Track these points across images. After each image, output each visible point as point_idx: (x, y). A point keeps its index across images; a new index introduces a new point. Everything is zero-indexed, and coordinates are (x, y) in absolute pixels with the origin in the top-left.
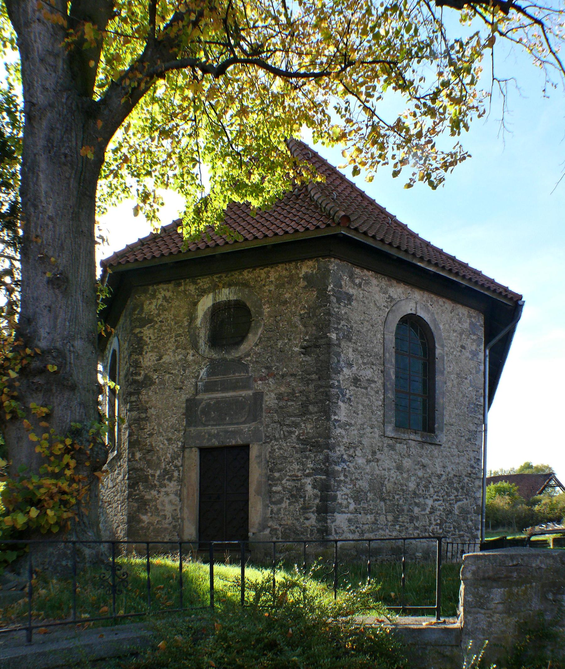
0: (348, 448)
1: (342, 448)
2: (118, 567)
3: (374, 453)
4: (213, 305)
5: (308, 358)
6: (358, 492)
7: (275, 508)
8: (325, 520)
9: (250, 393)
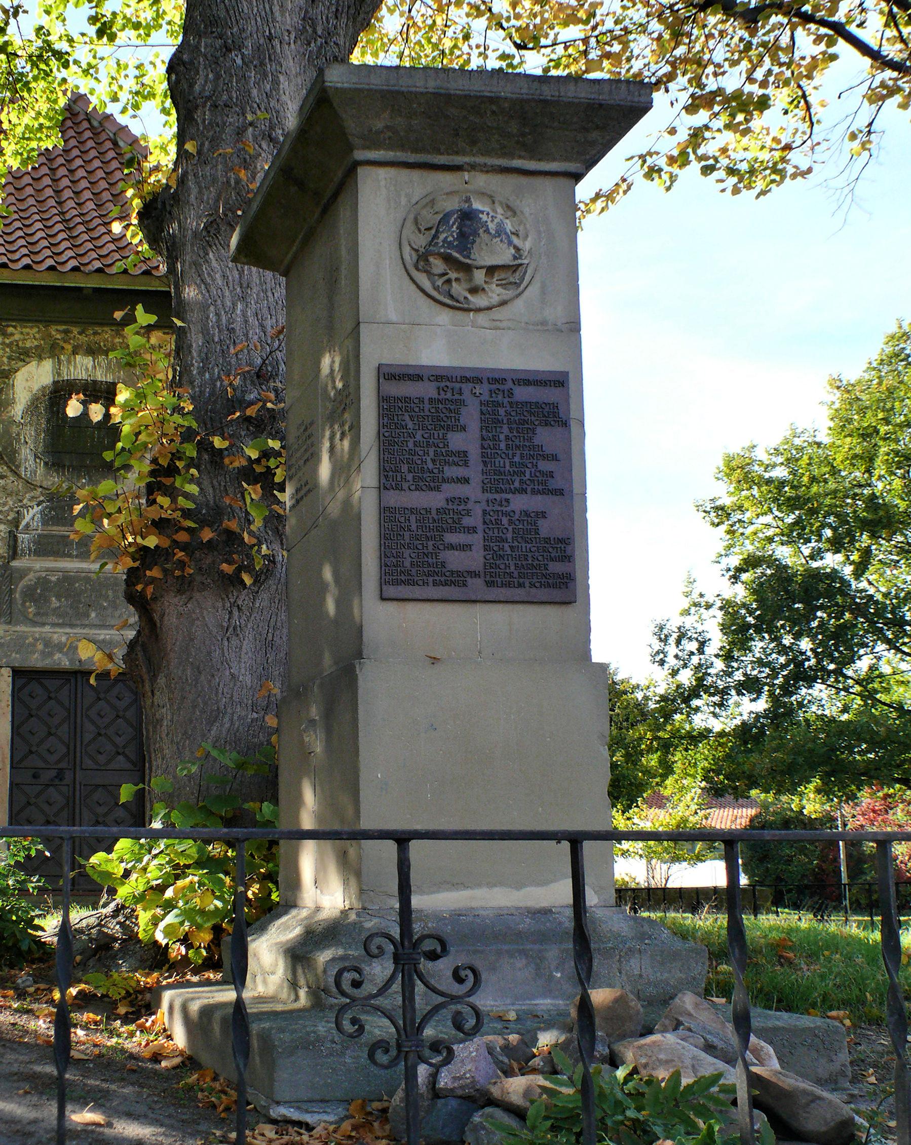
2: (429, 945)
4: (55, 383)
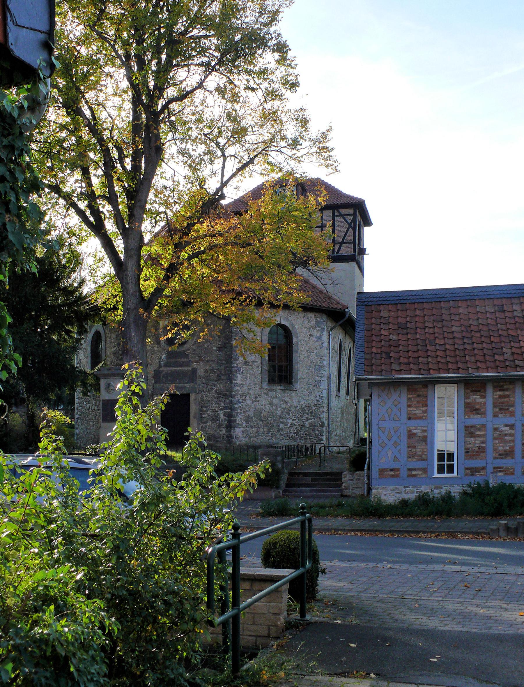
0: (242, 396)
1: (239, 397)
3: (256, 397)
5: (221, 353)
6: (248, 417)
7: (204, 425)
8: (230, 431)
9: (190, 368)
